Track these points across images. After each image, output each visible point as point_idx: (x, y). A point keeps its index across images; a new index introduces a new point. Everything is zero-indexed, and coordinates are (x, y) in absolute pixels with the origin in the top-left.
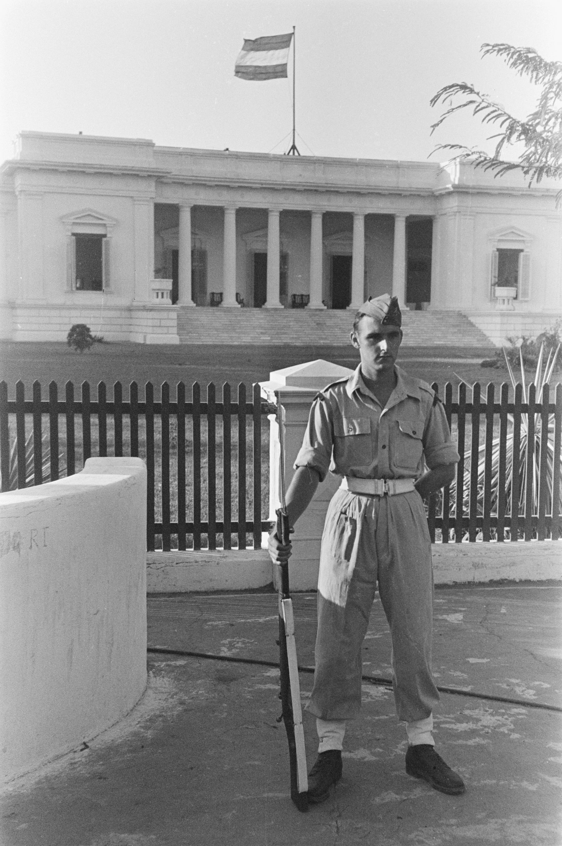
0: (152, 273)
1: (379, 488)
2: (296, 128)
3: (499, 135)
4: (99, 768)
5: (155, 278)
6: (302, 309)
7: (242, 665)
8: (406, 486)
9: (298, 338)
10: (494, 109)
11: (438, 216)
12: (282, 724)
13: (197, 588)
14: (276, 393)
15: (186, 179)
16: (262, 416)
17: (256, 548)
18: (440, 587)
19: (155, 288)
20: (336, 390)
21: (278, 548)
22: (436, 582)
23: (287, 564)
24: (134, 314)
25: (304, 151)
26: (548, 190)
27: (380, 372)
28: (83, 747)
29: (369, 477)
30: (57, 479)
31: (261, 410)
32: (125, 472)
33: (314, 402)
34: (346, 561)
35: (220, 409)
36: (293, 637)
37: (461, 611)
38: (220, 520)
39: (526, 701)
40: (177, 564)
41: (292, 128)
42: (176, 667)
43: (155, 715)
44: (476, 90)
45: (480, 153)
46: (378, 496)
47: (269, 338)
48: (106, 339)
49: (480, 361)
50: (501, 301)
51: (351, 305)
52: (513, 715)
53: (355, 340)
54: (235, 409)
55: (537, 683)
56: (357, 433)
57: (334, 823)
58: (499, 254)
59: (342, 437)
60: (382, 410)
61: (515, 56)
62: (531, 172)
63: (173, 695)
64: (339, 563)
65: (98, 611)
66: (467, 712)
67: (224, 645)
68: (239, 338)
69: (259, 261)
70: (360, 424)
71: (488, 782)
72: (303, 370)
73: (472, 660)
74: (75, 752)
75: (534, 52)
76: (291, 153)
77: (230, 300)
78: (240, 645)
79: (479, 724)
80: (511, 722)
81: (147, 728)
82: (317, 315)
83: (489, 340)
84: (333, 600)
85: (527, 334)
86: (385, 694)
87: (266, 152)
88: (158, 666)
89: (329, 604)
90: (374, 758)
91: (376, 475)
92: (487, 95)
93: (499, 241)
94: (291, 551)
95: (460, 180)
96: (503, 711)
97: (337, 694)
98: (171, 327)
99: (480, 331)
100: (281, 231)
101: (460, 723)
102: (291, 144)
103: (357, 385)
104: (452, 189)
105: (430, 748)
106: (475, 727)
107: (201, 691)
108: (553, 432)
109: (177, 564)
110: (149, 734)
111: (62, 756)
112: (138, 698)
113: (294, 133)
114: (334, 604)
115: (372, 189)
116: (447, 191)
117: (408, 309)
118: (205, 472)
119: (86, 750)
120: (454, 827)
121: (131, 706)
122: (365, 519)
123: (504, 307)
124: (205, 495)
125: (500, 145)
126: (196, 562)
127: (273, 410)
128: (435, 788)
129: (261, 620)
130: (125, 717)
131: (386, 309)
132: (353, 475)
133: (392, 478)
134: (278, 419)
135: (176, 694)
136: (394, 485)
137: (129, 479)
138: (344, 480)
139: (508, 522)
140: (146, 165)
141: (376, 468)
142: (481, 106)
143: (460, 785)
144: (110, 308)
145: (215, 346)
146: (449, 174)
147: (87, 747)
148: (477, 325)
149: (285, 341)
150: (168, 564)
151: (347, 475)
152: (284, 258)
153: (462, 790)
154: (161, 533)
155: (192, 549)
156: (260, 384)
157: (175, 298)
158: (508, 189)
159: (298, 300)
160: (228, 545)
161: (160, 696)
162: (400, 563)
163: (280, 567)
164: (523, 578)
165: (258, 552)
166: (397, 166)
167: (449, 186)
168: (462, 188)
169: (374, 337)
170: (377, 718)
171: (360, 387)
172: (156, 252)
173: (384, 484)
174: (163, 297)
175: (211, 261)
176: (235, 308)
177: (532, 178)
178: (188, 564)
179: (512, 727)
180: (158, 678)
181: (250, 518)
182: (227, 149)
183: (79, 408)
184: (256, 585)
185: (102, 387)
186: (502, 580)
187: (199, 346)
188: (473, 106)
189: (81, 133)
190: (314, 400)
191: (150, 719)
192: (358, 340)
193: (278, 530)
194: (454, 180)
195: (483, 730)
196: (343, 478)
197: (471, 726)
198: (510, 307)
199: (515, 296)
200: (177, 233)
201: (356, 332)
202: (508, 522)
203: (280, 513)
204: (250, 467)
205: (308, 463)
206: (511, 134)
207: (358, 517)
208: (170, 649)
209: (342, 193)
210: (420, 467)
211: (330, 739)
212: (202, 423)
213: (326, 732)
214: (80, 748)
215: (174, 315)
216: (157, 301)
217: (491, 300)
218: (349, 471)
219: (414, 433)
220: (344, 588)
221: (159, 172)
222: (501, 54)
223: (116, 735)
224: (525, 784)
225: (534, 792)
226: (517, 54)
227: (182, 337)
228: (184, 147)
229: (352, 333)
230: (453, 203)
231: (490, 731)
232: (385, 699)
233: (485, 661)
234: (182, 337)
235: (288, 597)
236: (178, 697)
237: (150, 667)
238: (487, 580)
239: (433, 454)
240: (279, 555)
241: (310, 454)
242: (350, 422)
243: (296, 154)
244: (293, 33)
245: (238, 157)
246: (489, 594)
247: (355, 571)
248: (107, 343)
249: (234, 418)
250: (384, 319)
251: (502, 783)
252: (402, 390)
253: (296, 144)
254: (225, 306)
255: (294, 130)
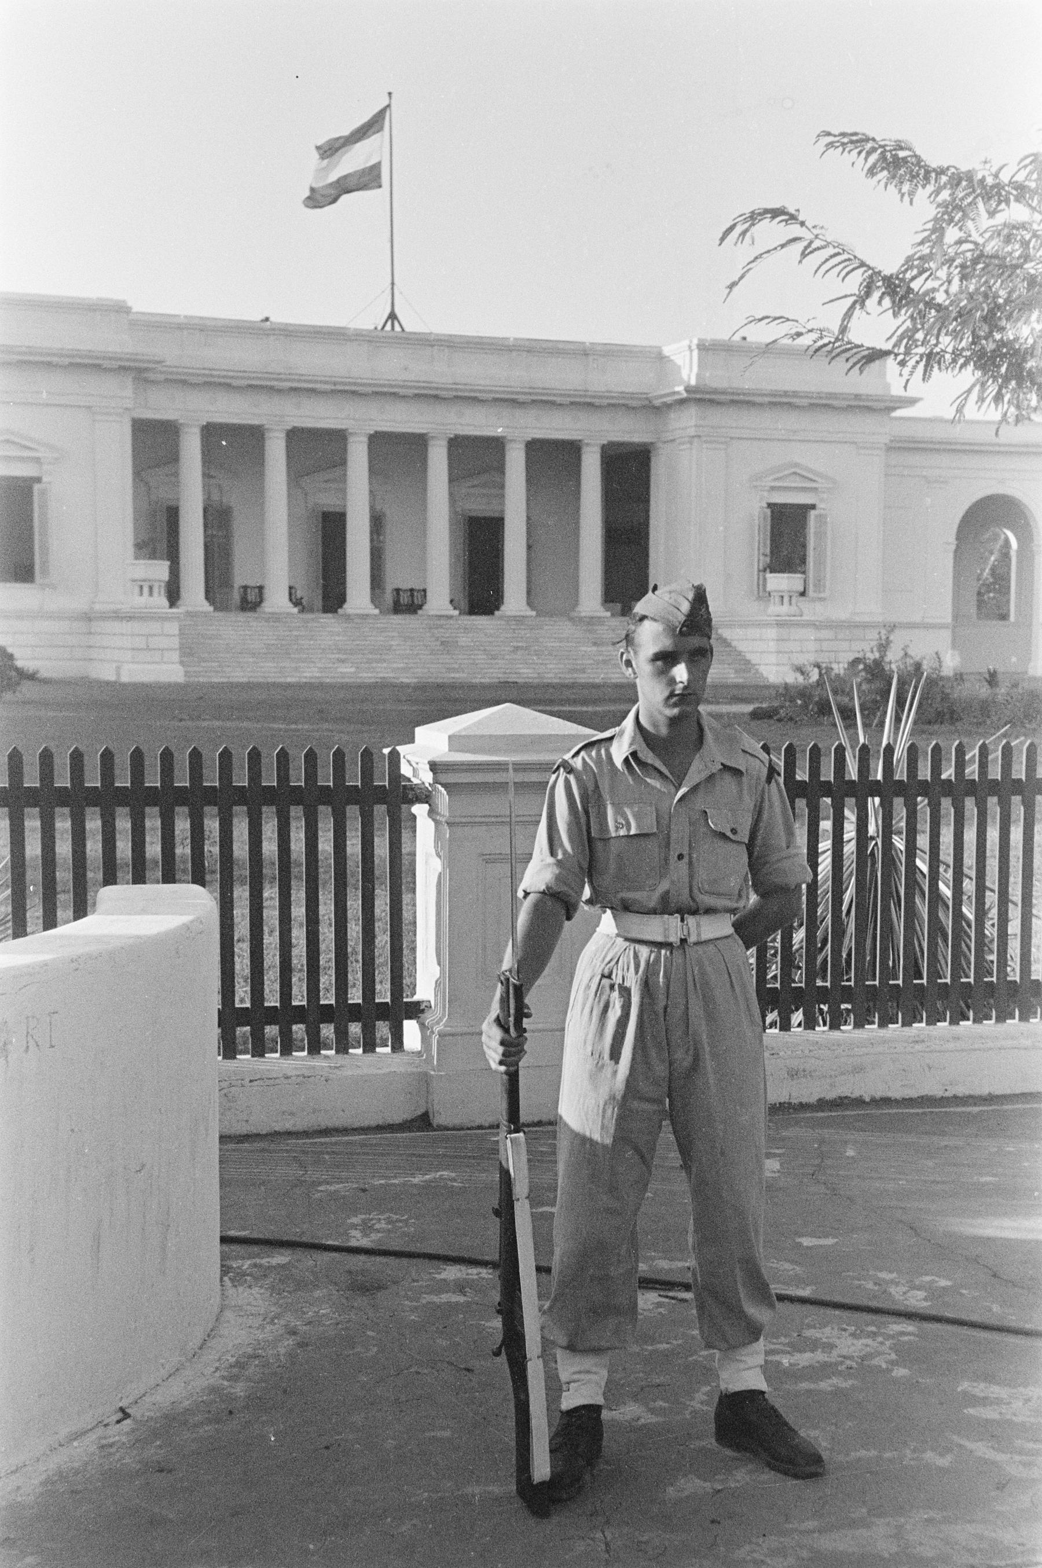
0: (130, 550)
1: (672, 931)
2: (396, 281)
3: (846, 296)
4: (154, 1452)
5: (136, 558)
6: (412, 617)
7: (391, 1261)
8: (720, 927)
9: (405, 669)
10: (837, 250)
11: (660, 445)
12: (503, 1359)
13: (288, 1125)
14: (434, 766)
15: (193, 375)
16: (404, 807)
17: (394, 1049)
18: (777, 1109)
19: (136, 577)
20: (594, 753)
21: (502, 1043)
22: (777, 1094)
23: (517, 1071)
24: (97, 626)
25: (411, 323)
26: (857, 397)
27: (673, 722)
28: (120, 1415)
29: (654, 912)
30: (55, 926)
31: (401, 795)
32: (179, 911)
33: (554, 777)
34: (613, 1062)
35: (326, 796)
36: (527, 1201)
37: (775, 1155)
38: (328, 999)
39: (909, 1309)
40: (251, 1081)
41: (390, 281)
42: (270, 1268)
43: (244, 1355)
44: (801, 218)
45: (821, 330)
46: (668, 945)
47: (353, 670)
48: (44, 674)
49: (749, 708)
50: (777, 599)
51: (503, 608)
52: (892, 1337)
53: (628, 663)
54: (354, 796)
55: (928, 1278)
56: (633, 832)
57: (599, 1535)
58: (772, 512)
59: (606, 840)
60: (677, 789)
61: (874, 157)
62: (911, 363)
63: (272, 1320)
64: (600, 1067)
65: (143, 1166)
66: (809, 1333)
67: (354, 1226)
68: (296, 669)
69: (332, 528)
70: (636, 816)
71: (863, 1453)
72: (479, 723)
73: (806, 1242)
74: (106, 1425)
75: (910, 149)
76: (388, 327)
77: (277, 600)
78: (383, 1225)
79: (835, 1353)
80: (890, 1348)
81: (234, 1378)
82: (441, 626)
83: (757, 670)
84: (588, 1134)
85: (823, 659)
86: (659, 1305)
87: (342, 325)
88: (238, 1267)
89: (583, 1141)
90: (653, 1419)
91: (665, 907)
92: (822, 227)
93: (773, 488)
94: (525, 1047)
95: (698, 376)
96: (873, 1329)
97: (594, 1305)
98: (167, 650)
99: (740, 653)
100: (372, 471)
101: (800, 1351)
102: (388, 311)
103: (631, 744)
104: (685, 395)
105: (761, 1397)
106: (826, 1359)
107: (323, 1309)
108: (901, 833)
109: (251, 1081)
110: (239, 1389)
111: (86, 1432)
112: (210, 1326)
113: (392, 289)
114: (591, 1140)
115: (536, 394)
116: (677, 397)
117: (608, 614)
118: (271, 915)
119: (128, 1421)
120: (816, 1535)
121: (198, 1342)
122: (647, 985)
123: (785, 609)
124: (272, 957)
125: (848, 314)
126: (287, 1078)
127: (424, 796)
128: (773, 1468)
129: (416, 1180)
130: (190, 1360)
131: (685, 607)
132: (624, 908)
133: (694, 912)
134: (432, 813)
135: (278, 1316)
136: (698, 925)
137: (192, 922)
138: (608, 917)
139: (847, 994)
140: (113, 348)
141: (665, 897)
142: (814, 246)
143: (818, 1460)
144: (51, 616)
145: (249, 686)
146: (679, 367)
147: (125, 1415)
148: (734, 644)
149: (381, 675)
150: (233, 1083)
151: (612, 908)
152: (377, 523)
153: (820, 1470)
154: (245, 1025)
155: (278, 1055)
156: (398, 748)
157: (173, 594)
158: (786, 394)
159: (405, 599)
160: (343, 1045)
161: (250, 1321)
162: (709, 1064)
163: (505, 1077)
164: (878, 1095)
165: (398, 1057)
166: (583, 352)
167: (680, 388)
168: (703, 392)
169: (665, 659)
170: (650, 1348)
171: (638, 749)
172: (136, 510)
173: (679, 923)
174: (151, 593)
175: (240, 527)
176: (288, 614)
177: (911, 373)
178: (272, 1082)
179: (893, 1356)
180: (241, 1289)
181: (383, 995)
182: (267, 319)
183: (93, 798)
184: (397, 1118)
185: (107, 757)
186: (840, 1098)
187: (221, 686)
188: (800, 246)
189: (744, 338)
190: (554, 772)
191: (237, 1362)
192: (634, 663)
193: (502, 1008)
194: (689, 376)
195: (842, 1363)
196: (605, 912)
197: (820, 1356)
198: (793, 609)
199: (802, 590)
200: (176, 474)
201: (630, 649)
202: (847, 994)
203: (508, 980)
204: (1017, 834)
205: (548, 888)
206: (868, 294)
207: (633, 982)
208: (255, 1235)
209: (445, 399)
210: (744, 894)
211: (583, 1385)
212: (293, 824)
213: (574, 1373)
214: (115, 1418)
215: (173, 628)
216: (141, 601)
217: (759, 598)
218: (616, 902)
219: (734, 831)
220: (609, 1112)
221: (141, 361)
222: (849, 152)
223: (176, 1393)
224: (929, 1455)
225: (940, 1469)
226: (879, 151)
227: (189, 669)
228: (186, 313)
229: (622, 650)
230: (686, 421)
231: (854, 1365)
232: (660, 1313)
233: (830, 1241)
234: (189, 669)
235: (517, 1131)
236: (283, 1322)
237: (225, 1270)
238: (813, 1099)
239: (764, 871)
240: (503, 1055)
241: (550, 870)
242: (619, 812)
243: (397, 328)
244: (389, 106)
245: (290, 333)
246: (822, 1124)
247: (630, 1082)
248: (46, 681)
249: (325, 812)
250: (683, 626)
251: (888, 1455)
252: (713, 754)
253: (397, 311)
254: (267, 610)
255: (393, 284)
